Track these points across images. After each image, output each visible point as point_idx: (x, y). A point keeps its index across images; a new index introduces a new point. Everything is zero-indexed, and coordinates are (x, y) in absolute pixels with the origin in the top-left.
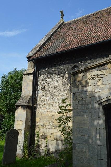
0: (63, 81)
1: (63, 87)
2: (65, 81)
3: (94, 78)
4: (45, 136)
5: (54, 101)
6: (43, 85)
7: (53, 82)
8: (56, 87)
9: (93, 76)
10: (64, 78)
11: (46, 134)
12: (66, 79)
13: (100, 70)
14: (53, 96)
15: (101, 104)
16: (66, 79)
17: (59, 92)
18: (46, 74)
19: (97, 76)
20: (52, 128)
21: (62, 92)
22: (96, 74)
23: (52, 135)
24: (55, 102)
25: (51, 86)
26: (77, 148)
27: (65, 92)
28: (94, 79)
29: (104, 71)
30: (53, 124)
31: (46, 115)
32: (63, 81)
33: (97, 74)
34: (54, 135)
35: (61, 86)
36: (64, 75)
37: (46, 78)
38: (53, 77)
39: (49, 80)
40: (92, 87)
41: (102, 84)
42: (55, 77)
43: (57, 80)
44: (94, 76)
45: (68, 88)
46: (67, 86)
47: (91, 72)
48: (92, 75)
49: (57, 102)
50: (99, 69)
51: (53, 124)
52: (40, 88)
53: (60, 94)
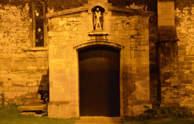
0: (22, 14)
1: (23, 22)
5: (9, 39)
7: (6, 14)
8: (13, 22)
9: (69, 22)
10: (24, 11)
12: (27, 13)
14: (8, 34)
16: (27, 13)
17: (16, 28)
19: (72, 23)
20: (9, 73)
22: (72, 21)
23: (10, 81)
24: (11, 41)
26: (54, 86)
27: (25, 29)
28: (70, 25)
29: (79, 19)
30: (10, 67)
32: (22, 15)
33: (73, 21)
35: (20, 21)
38: (6, 7)
41: (77, 30)
42: (10, 7)
44: (70, 22)
45: (29, 25)
46: (28, 21)
48: (69, 21)
51: (9, 68)
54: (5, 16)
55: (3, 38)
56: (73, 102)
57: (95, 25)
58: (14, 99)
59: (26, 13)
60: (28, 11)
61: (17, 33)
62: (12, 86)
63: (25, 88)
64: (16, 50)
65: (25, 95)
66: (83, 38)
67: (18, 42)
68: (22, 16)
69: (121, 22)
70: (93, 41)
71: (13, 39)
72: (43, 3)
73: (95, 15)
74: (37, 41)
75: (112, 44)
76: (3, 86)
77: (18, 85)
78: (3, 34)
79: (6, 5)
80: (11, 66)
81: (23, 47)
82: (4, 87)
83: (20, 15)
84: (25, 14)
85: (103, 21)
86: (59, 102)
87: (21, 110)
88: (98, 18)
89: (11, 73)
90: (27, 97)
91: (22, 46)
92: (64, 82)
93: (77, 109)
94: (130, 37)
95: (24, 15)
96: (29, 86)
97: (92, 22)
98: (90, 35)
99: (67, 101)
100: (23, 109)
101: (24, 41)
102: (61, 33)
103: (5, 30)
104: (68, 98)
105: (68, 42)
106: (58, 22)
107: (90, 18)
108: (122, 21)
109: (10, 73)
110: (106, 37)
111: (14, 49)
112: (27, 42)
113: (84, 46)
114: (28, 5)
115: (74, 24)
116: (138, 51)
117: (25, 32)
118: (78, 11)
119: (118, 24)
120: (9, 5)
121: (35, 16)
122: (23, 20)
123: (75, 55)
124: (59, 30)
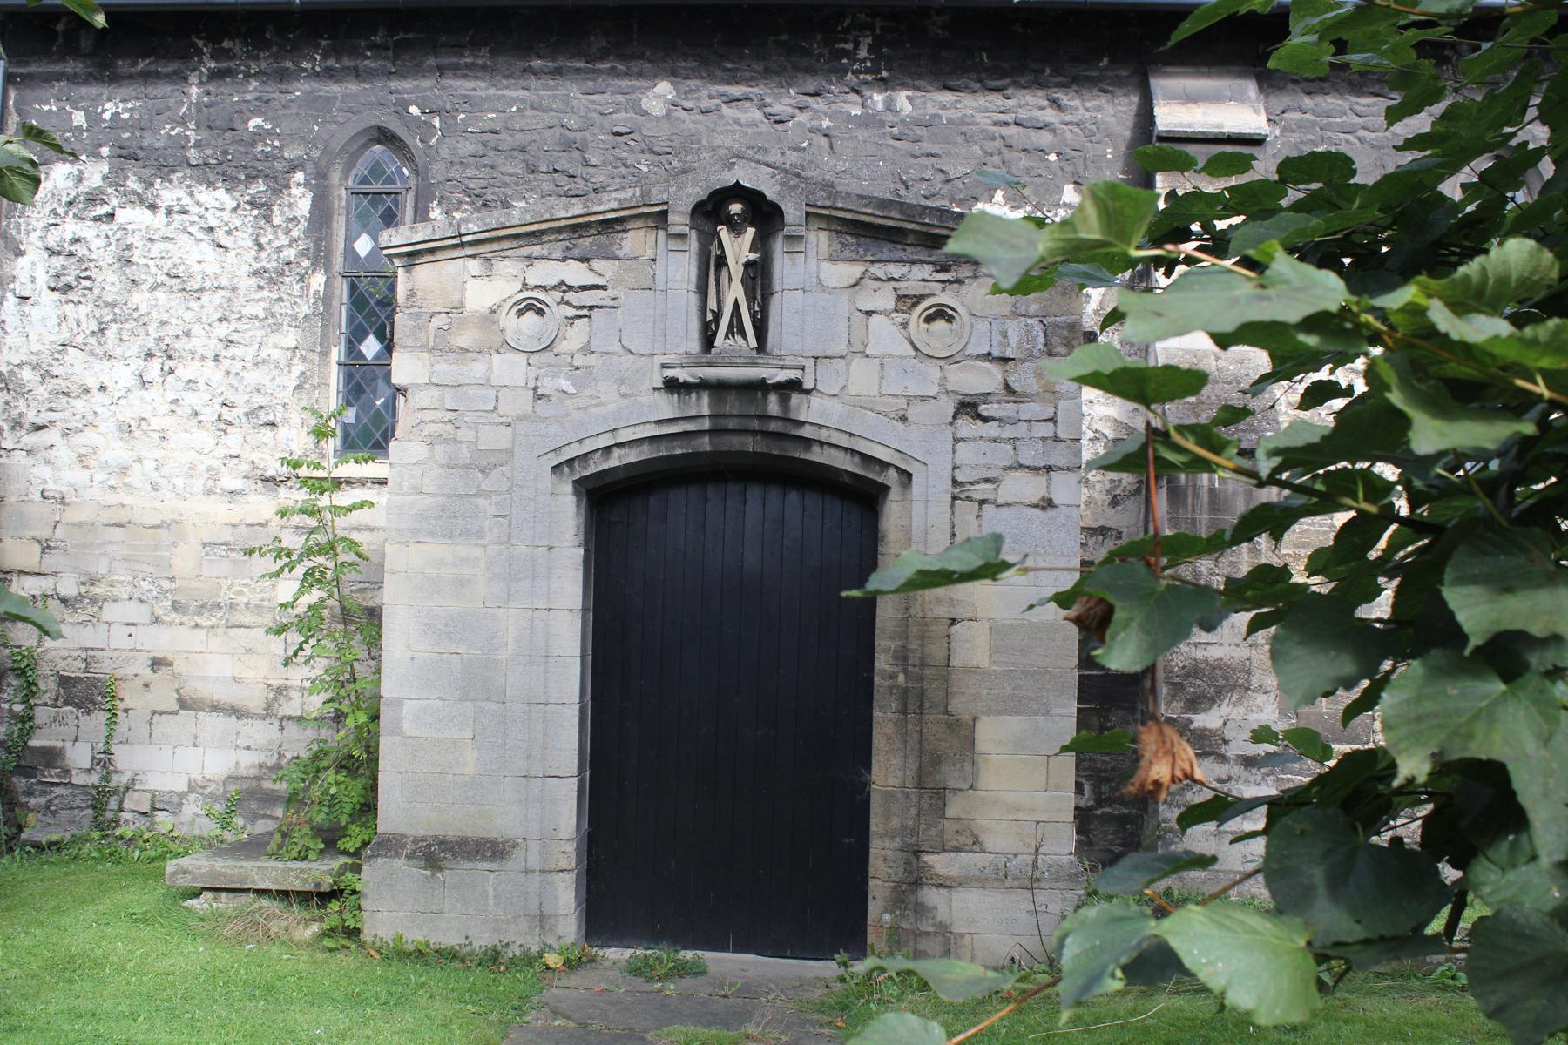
0: (264, 240)
1: (266, 293)
2: (287, 244)
3: (541, 301)
4: (93, 683)
5: (176, 401)
6: (71, 254)
8: (202, 290)
9: (537, 287)
10: (277, 220)
11: (103, 669)
12: (295, 233)
13: (582, 260)
14: (171, 363)
15: (566, 469)
16: (295, 233)
17: (223, 330)
18: (97, 156)
20: (156, 620)
21: (256, 332)
22: (554, 282)
23: (163, 672)
24: (184, 411)
25: (154, 270)
27: (275, 338)
28: (540, 312)
29: (606, 269)
30: (166, 585)
31: (107, 517)
32: (260, 247)
33: (562, 283)
34: (176, 676)
35: (246, 283)
36: (277, 192)
37: (100, 190)
38: (168, 194)
39: (133, 216)
40: (522, 358)
41: (587, 350)
42: (191, 194)
43: (211, 229)
44: (544, 288)
45: (305, 310)
46: (296, 287)
47: (529, 257)
48: (532, 282)
49: (209, 415)
50: (576, 253)
51: (164, 592)
52: (43, 279)
53: (232, 350)
54: (156, 249)
55: (139, 393)
56: (534, 847)
57: (710, 317)
58: (183, 795)
59: (287, 233)
60: (303, 224)
61: (226, 364)
62: (176, 707)
63: (258, 724)
64: (214, 474)
65: (253, 772)
66: (625, 402)
67: (230, 424)
68: (264, 255)
69: (891, 305)
70: (691, 427)
71: (193, 400)
72: (405, 171)
73: (715, 251)
74: (350, 415)
75: (827, 450)
76: (118, 702)
77: (215, 707)
78: (133, 367)
79: (166, 179)
80: (172, 579)
81: (254, 456)
82: (126, 711)
83: (250, 243)
84: (284, 240)
85: (767, 293)
86: (441, 843)
87: (182, 881)
88: (736, 269)
89: (171, 624)
90: (267, 785)
91: (323, 456)
92: (482, 704)
93: (565, 897)
94: (951, 411)
95: (277, 244)
96: (281, 714)
97: (694, 299)
98: (672, 386)
99: (493, 835)
100: (194, 879)
101: (264, 418)
102: (477, 369)
103: (151, 343)
104: (503, 821)
105: (522, 427)
106: (463, 290)
107: (681, 267)
108: (899, 298)
109: (163, 622)
110: (784, 401)
111: (203, 468)
112: (286, 421)
113: (632, 456)
114: (307, 184)
115: (568, 303)
116: (1005, 509)
117: (277, 354)
118: (601, 217)
119: (869, 313)
120: (185, 177)
121: (350, 253)
122: (270, 278)
123: (565, 516)
124: (464, 340)
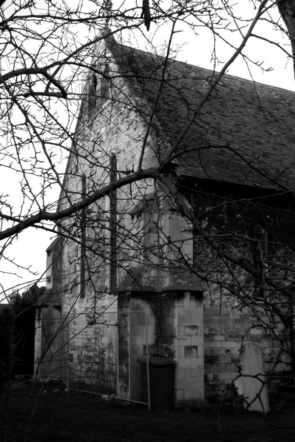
4: (213, 357)
20: (226, 340)
34: (232, 354)
